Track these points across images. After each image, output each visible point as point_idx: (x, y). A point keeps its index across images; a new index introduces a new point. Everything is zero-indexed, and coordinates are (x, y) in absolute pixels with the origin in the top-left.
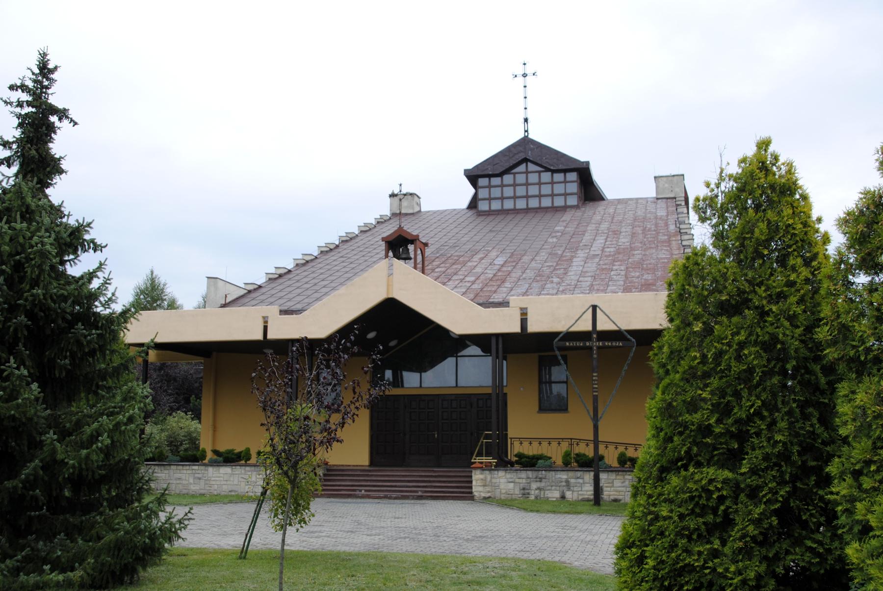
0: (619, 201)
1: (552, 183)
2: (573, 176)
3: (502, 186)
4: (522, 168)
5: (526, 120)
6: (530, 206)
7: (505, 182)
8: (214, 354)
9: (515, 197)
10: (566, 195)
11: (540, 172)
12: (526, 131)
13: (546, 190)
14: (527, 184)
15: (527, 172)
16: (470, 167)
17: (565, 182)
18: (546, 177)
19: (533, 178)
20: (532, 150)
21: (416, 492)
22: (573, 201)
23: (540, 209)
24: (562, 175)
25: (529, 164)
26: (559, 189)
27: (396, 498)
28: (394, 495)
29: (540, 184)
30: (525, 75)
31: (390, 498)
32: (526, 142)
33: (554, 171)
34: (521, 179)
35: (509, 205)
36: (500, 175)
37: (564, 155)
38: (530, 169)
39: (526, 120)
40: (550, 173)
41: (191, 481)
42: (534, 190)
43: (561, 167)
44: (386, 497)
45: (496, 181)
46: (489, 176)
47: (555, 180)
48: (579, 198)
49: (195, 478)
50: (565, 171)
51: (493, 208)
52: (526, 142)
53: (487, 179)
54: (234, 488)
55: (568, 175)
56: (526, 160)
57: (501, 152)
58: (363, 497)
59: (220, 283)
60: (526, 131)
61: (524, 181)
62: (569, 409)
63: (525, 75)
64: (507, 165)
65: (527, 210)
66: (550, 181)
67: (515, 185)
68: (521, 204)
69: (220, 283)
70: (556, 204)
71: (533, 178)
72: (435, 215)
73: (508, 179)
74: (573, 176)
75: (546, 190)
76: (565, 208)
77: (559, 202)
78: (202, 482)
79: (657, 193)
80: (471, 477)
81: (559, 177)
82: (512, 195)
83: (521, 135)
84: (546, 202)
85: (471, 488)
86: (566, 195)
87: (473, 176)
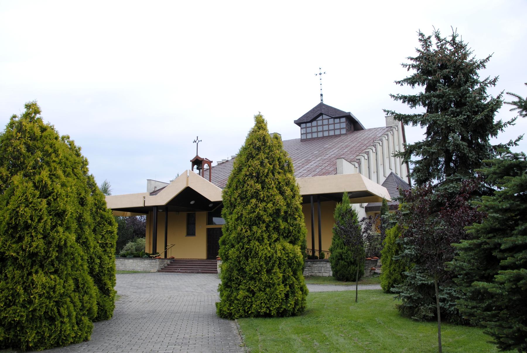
0: (370, 130)
1: (334, 124)
2: (343, 120)
3: (312, 127)
4: (320, 118)
5: (322, 95)
6: (325, 135)
7: (313, 125)
8: (149, 212)
9: (317, 132)
10: (340, 129)
11: (328, 119)
12: (322, 100)
13: (331, 127)
14: (323, 125)
15: (323, 120)
16: (297, 119)
17: (340, 123)
18: (331, 121)
19: (325, 122)
20: (324, 109)
21: (176, 269)
22: (344, 131)
23: (318, 138)
24: (305, 124)
25: (324, 115)
26: (337, 126)
27: (189, 273)
28: (189, 271)
29: (328, 125)
30: (320, 74)
31: (187, 273)
32: (321, 105)
33: (334, 118)
34: (320, 123)
35: (315, 135)
36: (311, 121)
37: (338, 110)
38: (324, 118)
39: (322, 95)
40: (333, 119)
41: (120, 265)
42: (326, 128)
43: (337, 116)
44: (185, 272)
45: (309, 125)
46: (306, 123)
47: (335, 122)
48: (347, 130)
49: (121, 264)
50: (340, 118)
51: (308, 137)
52: (321, 105)
53: (305, 124)
54: (134, 268)
55: (341, 119)
56: (321, 114)
57: (310, 111)
58: (179, 272)
59: (153, 182)
60: (322, 100)
61: (321, 124)
62: (196, 234)
63: (320, 74)
64: (313, 117)
65: (323, 137)
66: (333, 123)
67: (317, 126)
68: (320, 135)
69: (153, 182)
70: (336, 134)
71: (325, 122)
72: (379, 129)
73: (314, 123)
74: (343, 120)
75: (331, 127)
76: (340, 135)
77: (337, 132)
78: (123, 266)
79: (387, 125)
80: (217, 264)
81: (337, 121)
82: (310, 131)
83: (319, 102)
84: (332, 133)
85: (217, 268)
86: (340, 129)
87: (299, 123)
